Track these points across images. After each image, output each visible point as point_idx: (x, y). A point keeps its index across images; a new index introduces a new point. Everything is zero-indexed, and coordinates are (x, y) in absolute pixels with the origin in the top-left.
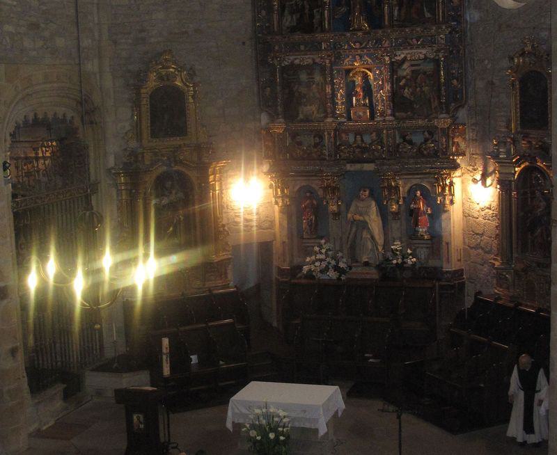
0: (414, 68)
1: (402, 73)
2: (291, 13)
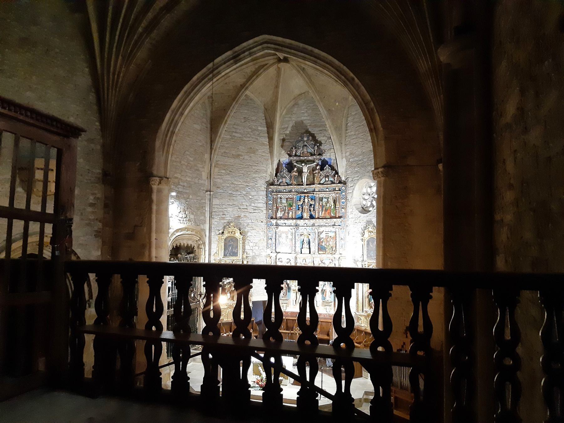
0: (327, 235)
1: (321, 236)
2: (281, 212)
